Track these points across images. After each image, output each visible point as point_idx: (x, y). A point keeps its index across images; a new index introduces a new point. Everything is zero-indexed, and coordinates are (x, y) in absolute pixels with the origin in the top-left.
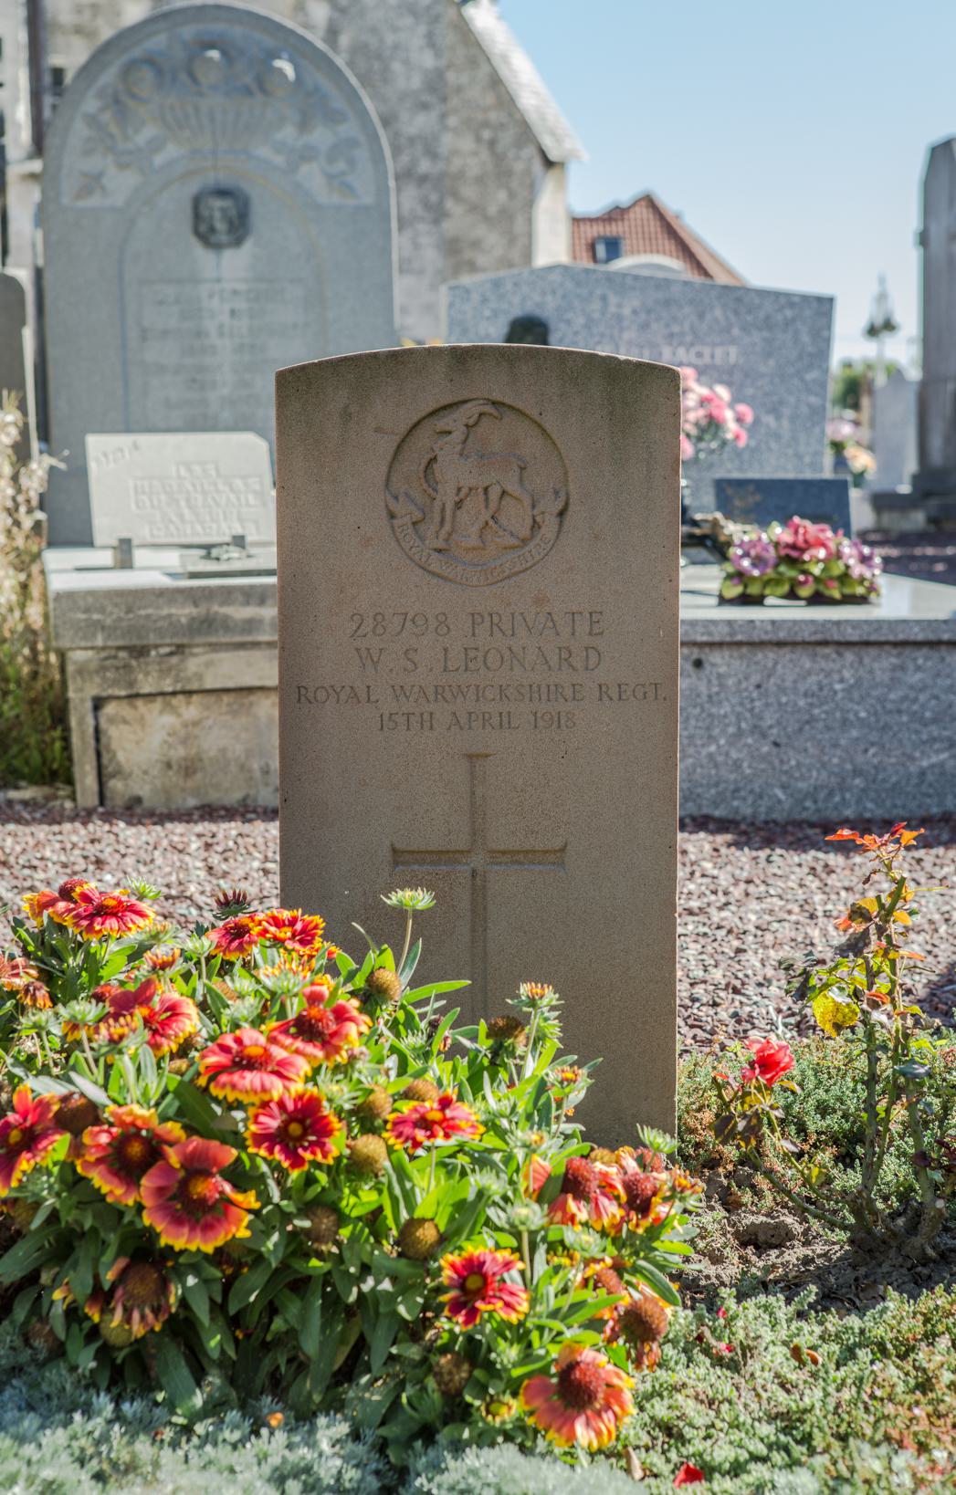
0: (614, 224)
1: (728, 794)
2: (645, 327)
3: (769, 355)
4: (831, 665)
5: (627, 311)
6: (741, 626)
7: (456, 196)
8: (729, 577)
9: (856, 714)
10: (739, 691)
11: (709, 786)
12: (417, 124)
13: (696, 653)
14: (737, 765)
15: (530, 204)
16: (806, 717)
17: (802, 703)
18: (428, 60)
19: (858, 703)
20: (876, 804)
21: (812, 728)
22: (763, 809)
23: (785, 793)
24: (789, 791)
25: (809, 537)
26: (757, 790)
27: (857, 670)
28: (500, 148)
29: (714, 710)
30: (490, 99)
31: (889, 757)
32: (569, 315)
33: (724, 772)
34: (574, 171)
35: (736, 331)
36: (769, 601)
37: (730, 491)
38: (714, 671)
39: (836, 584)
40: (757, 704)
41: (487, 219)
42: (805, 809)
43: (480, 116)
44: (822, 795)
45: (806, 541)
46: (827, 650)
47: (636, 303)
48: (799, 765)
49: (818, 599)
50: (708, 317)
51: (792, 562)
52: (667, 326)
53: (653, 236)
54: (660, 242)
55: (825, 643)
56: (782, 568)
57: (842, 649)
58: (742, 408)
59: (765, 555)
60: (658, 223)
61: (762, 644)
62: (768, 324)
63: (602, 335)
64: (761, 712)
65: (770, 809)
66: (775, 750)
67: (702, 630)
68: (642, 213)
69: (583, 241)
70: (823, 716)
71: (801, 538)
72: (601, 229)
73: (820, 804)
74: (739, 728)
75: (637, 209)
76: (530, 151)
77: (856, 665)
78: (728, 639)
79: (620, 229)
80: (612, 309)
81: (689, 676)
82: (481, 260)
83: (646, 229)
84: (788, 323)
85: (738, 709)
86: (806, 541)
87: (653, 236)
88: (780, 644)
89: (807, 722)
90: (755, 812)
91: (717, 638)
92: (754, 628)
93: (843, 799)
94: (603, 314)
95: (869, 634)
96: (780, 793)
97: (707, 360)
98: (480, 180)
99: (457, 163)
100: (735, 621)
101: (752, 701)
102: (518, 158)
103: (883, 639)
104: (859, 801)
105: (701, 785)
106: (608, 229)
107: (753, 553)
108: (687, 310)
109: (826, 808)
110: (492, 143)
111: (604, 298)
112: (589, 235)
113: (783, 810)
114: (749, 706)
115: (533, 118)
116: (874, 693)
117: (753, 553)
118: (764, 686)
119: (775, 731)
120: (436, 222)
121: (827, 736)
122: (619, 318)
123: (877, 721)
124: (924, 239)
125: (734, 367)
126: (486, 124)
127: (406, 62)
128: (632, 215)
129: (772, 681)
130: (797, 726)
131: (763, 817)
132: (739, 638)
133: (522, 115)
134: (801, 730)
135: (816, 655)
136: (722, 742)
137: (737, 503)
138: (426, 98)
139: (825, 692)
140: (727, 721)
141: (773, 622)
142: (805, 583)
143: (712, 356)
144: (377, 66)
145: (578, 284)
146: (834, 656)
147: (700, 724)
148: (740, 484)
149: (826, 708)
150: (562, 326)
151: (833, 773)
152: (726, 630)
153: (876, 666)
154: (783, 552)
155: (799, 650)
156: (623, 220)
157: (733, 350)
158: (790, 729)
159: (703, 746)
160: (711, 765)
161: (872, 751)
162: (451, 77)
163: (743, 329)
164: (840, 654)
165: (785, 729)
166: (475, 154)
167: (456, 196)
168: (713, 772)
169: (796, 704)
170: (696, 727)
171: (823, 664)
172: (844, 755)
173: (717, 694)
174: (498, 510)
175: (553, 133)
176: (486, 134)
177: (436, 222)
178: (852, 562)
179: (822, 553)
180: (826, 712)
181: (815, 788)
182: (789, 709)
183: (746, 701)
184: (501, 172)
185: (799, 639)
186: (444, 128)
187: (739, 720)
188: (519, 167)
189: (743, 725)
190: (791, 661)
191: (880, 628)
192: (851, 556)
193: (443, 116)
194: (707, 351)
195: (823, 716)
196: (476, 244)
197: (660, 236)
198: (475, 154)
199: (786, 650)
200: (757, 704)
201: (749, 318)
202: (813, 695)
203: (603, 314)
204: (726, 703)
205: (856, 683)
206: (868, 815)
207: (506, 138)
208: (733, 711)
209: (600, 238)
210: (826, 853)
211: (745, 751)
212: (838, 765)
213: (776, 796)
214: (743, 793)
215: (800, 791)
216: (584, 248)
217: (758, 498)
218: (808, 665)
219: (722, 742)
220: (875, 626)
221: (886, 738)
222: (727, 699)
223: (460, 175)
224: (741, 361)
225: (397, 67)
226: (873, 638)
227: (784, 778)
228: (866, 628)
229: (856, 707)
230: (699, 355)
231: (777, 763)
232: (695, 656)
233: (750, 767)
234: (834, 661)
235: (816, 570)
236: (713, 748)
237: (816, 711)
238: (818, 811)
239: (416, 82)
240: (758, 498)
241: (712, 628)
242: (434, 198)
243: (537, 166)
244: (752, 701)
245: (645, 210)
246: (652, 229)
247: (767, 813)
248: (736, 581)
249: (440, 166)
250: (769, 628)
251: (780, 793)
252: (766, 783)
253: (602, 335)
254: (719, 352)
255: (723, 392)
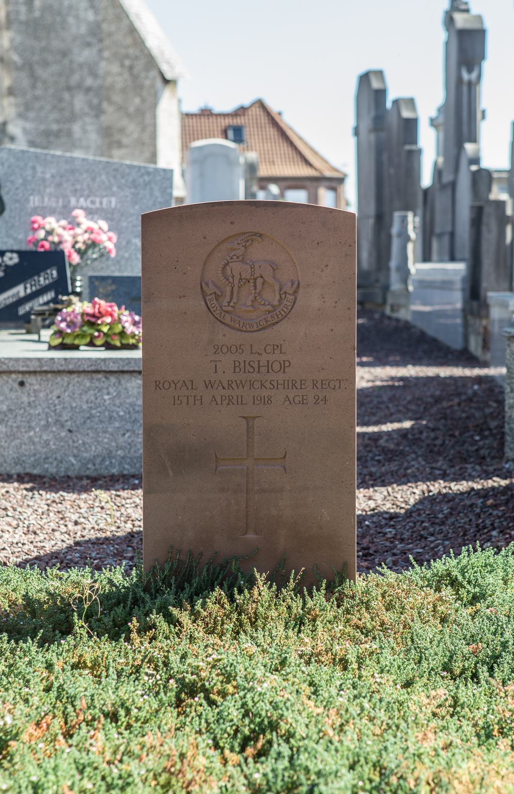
0: (238, 118)
1: (42, 460)
2: (59, 185)
3: (136, 203)
4: (102, 384)
5: (48, 176)
6: (46, 362)
7: (109, 100)
8: (55, 333)
9: (117, 413)
10: (47, 400)
11: (30, 456)
12: (84, 55)
13: (20, 378)
14: (47, 443)
15: (154, 105)
16: (88, 415)
17: (85, 407)
18: (90, 16)
19: (119, 407)
20: (131, 466)
21: (91, 421)
22: (63, 469)
23: (76, 460)
24: (78, 458)
25: (101, 310)
26: (59, 458)
27: (118, 388)
28: (135, 71)
29: (32, 411)
30: (129, 41)
31: (138, 438)
32: (12, 178)
33: (39, 447)
34: (181, 85)
35: (115, 189)
36: (82, 348)
37: (97, 283)
38: (32, 388)
39: (117, 338)
40: (58, 407)
41: (128, 115)
42: (88, 469)
43: (123, 51)
44: (98, 461)
45: (100, 312)
46: (100, 376)
47: (54, 171)
48: (84, 443)
49: (109, 346)
50: (98, 180)
51: (92, 324)
52: (73, 185)
53: (263, 125)
54: (268, 129)
55: (97, 372)
56: (85, 328)
57: (108, 375)
58: (111, 234)
59: (75, 320)
60: (266, 118)
61: (59, 372)
62: (134, 184)
63: (33, 190)
64: (61, 412)
65: (67, 469)
66: (69, 435)
67: (23, 364)
68: (257, 111)
69: (219, 128)
70: (98, 414)
71: (97, 311)
72: (231, 121)
73: (97, 466)
74: (48, 422)
75: (253, 109)
76: (154, 73)
77: (117, 384)
78: (38, 369)
79: (243, 121)
80: (39, 174)
81: (17, 391)
82: (125, 141)
83: (259, 121)
84: (146, 184)
85: (47, 410)
86: (100, 312)
87: (263, 125)
88: (71, 372)
89: (89, 418)
90: (58, 471)
91: (32, 369)
92: (54, 363)
93: (111, 463)
94: (34, 177)
95: (123, 366)
96: (73, 460)
97: (98, 205)
98: (123, 91)
99: (109, 80)
100: (43, 359)
101: (55, 406)
102: (147, 78)
103: (131, 369)
104: (120, 464)
105: (25, 455)
106: (239, 121)
107: (68, 319)
108: (85, 176)
109: (101, 469)
110: (131, 68)
111: (34, 168)
112: (223, 125)
113: (75, 469)
114: (53, 409)
115: (155, 52)
116: (128, 401)
117: (68, 319)
118: (62, 397)
119: (69, 423)
120: (97, 116)
121: (101, 426)
122: (44, 180)
123: (130, 417)
124: (357, 132)
125: (115, 209)
126: (127, 56)
127: (77, 17)
128: (250, 112)
129: (67, 394)
130: (82, 421)
131: (62, 474)
132: (45, 368)
133: (149, 51)
134: (84, 422)
135: (93, 379)
136: (37, 430)
137: (101, 290)
138: (89, 39)
139: (99, 400)
140: (40, 417)
141: (66, 359)
142: (99, 336)
143: (101, 203)
144: (58, 19)
145: (18, 159)
146: (104, 379)
147: (24, 419)
148: (103, 279)
149: (99, 409)
150: (8, 184)
151: (105, 448)
152: (37, 364)
153: (129, 385)
154: (86, 318)
155: (82, 376)
156: (244, 115)
157: (113, 200)
158: (78, 422)
159: (26, 432)
160: (31, 444)
161: (127, 435)
162: (105, 26)
163: (119, 187)
164: (106, 378)
165: (75, 422)
166: (120, 74)
167: (109, 100)
168: (32, 447)
169: (81, 407)
170: (21, 421)
171: (97, 384)
172: (111, 437)
173: (34, 401)
174: (261, 291)
175: (168, 63)
176: (127, 63)
177: (97, 116)
178: (127, 325)
179: (108, 320)
180: (99, 412)
181: (94, 457)
182: (77, 410)
183: (52, 406)
184: (137, 87)
185: (81, 369)
186: (102, 58)
187: (47, 418)
188: (147, 83)
189: (50, 420)
190: (78, 382)
191: (130, 363)
192: (126, 321)
193: (100, 51)
194: (98, 200)
195: (98, 414)
196: (122, 130)
197: (267, 125)
198: (120, 74)
199: (74, 376)
200: (58, 407)
201: (123, 181)
202: (91, 402)
203: (34, 177)
204: (39, 407)
205: (117, 395)
206: (126, 472)
207: (140, 65)
208: (43, 412)
209: (229, 126)
210: (68, 493)
211: (51, 435)
212: (107, 443)
213: (70, 461)
214: (50, 460)
215: (85, 458)
216: (220, 133)
217: (114, 287)
218: (88, 384)
219: (37, 430)
220: (127, 361)
221: (135, 427)
222: (40, 405)
223: (111, 87)
224: (119, 206)
225: (71, 20)
226: (126, 369)
227: (75, 451)
228: (121, 363)
229: (118, 409)
230: (93, 202)
231: (71, 442)
232: (20, 380)
233: (54, 444)
234: (103, 382)
235: (105, 329)
236: (32, 433)
237: (94, 412)
238: (96, 470)
239: (83, 30)
240: (114, 287)
241: (29, 363)
242: (95, 101)
243: (159, 83)
244: (55, 406)
245: (258, 109)
246: (263, 121)
247: (65, 472)
248: (57, 336)
249: (99, 82)
250: (63, 363)
251: (73, 460)
252: (65, 454)
253: (33, 190)
254: (105, 201)
255: (104, 225)
